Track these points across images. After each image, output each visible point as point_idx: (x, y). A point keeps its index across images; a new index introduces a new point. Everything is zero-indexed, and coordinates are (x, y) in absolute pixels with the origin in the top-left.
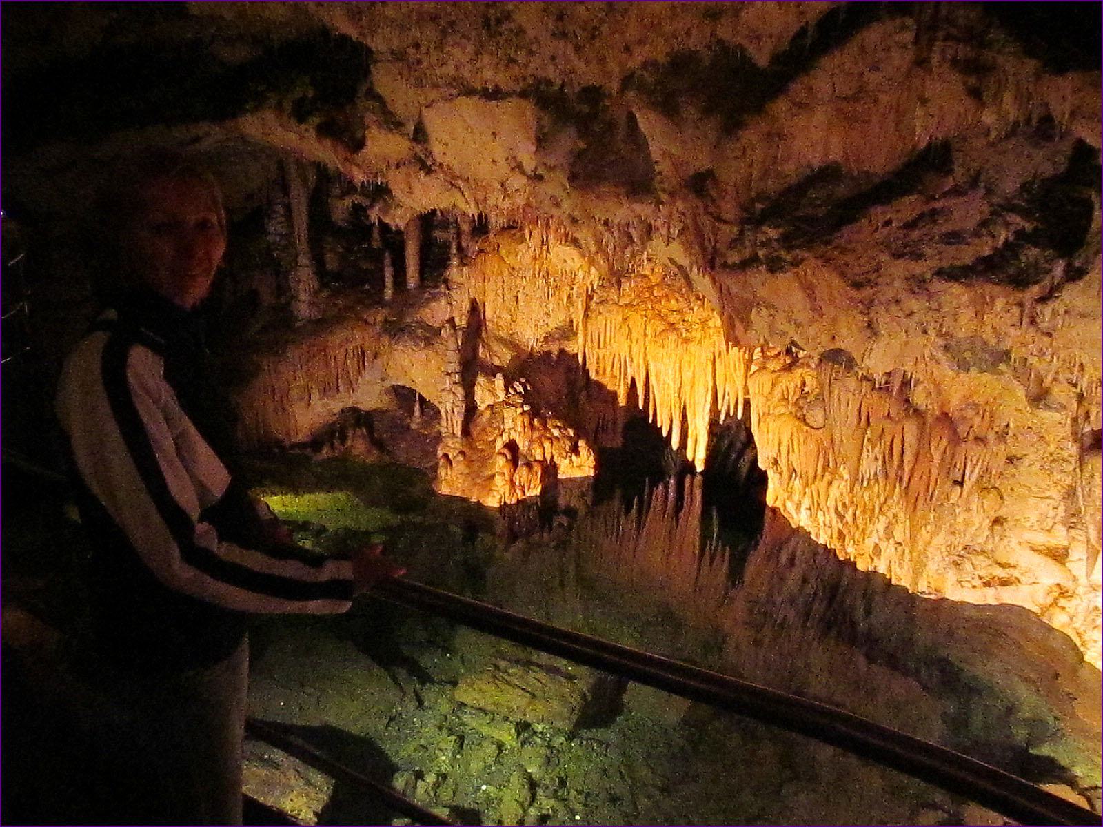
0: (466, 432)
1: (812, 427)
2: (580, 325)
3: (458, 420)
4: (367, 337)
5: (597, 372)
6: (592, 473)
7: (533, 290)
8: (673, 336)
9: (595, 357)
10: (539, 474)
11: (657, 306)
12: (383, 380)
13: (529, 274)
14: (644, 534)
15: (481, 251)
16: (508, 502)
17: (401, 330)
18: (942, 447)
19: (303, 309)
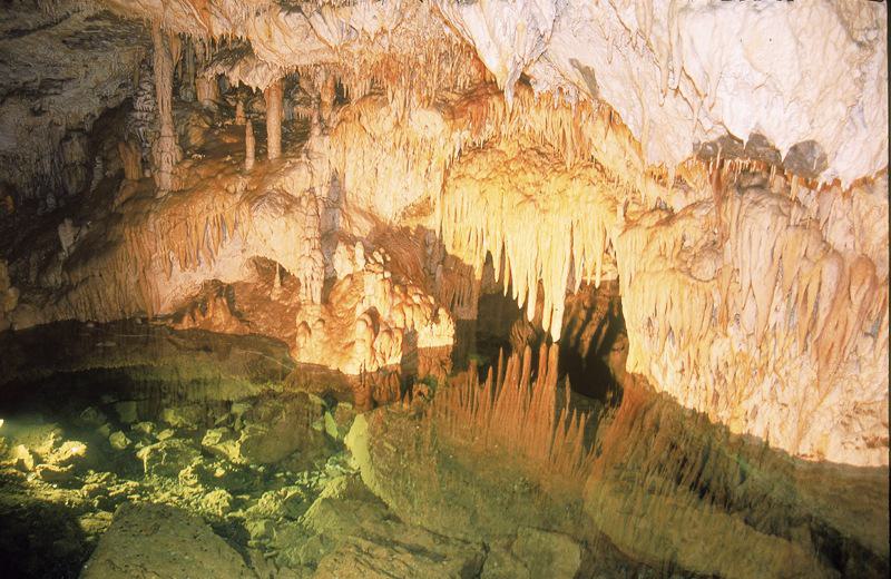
0: (326, 301)
1: (700, 280)
2: (438, 199)
3: (318, 286)
4: (227, 206)
5: (454, 247)
6: (451, 342)
7: (393, 164)
8: (530, 207)
9: (452, 231)
10: (400, 341)
11: (515, 180)
12: (243, 251)
13: (389, 144)
14: (499, 403)
15: (343, 120)
16: (368, 370)
17: (260, 197)
18: (863, 291)
19: (166, 180)
